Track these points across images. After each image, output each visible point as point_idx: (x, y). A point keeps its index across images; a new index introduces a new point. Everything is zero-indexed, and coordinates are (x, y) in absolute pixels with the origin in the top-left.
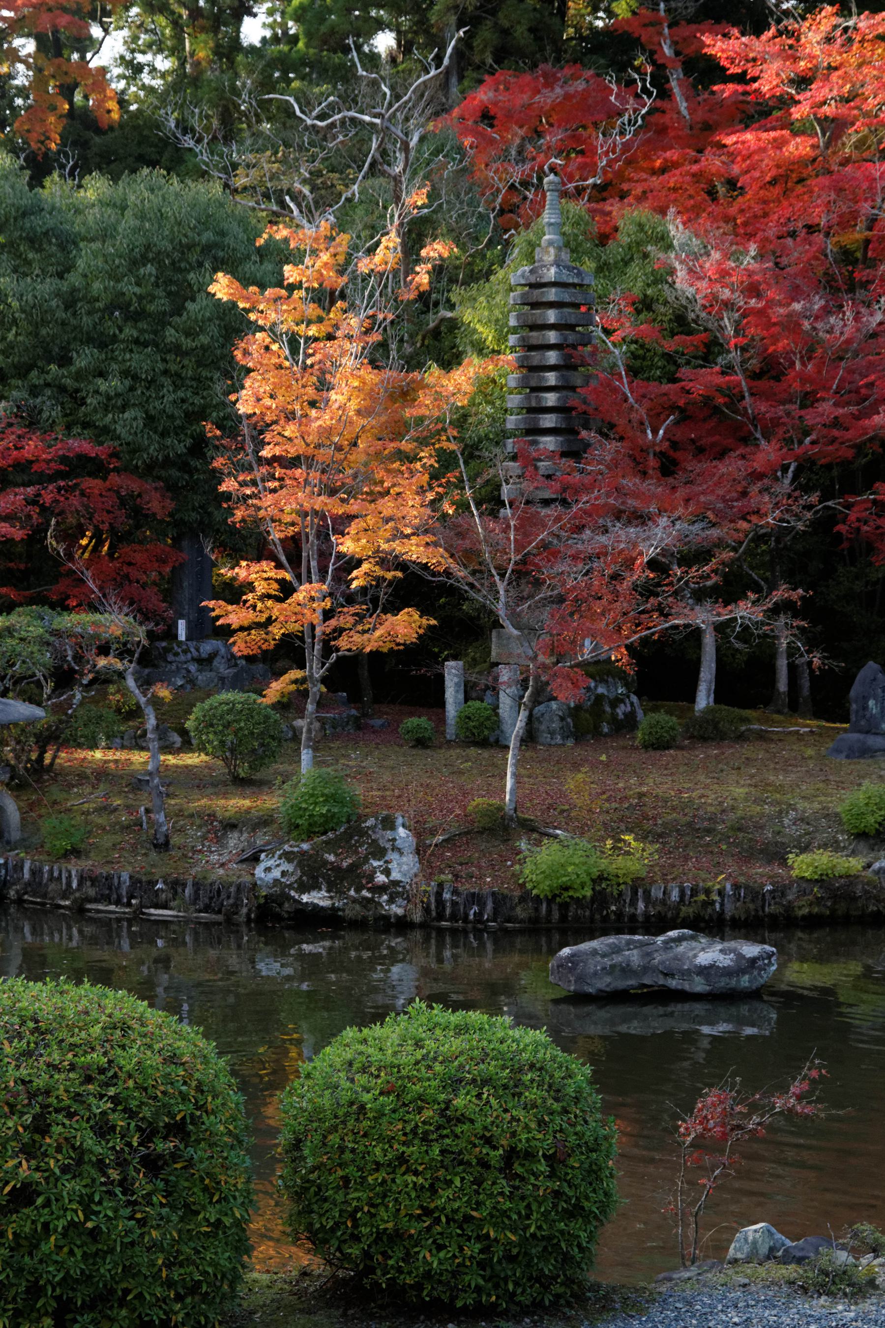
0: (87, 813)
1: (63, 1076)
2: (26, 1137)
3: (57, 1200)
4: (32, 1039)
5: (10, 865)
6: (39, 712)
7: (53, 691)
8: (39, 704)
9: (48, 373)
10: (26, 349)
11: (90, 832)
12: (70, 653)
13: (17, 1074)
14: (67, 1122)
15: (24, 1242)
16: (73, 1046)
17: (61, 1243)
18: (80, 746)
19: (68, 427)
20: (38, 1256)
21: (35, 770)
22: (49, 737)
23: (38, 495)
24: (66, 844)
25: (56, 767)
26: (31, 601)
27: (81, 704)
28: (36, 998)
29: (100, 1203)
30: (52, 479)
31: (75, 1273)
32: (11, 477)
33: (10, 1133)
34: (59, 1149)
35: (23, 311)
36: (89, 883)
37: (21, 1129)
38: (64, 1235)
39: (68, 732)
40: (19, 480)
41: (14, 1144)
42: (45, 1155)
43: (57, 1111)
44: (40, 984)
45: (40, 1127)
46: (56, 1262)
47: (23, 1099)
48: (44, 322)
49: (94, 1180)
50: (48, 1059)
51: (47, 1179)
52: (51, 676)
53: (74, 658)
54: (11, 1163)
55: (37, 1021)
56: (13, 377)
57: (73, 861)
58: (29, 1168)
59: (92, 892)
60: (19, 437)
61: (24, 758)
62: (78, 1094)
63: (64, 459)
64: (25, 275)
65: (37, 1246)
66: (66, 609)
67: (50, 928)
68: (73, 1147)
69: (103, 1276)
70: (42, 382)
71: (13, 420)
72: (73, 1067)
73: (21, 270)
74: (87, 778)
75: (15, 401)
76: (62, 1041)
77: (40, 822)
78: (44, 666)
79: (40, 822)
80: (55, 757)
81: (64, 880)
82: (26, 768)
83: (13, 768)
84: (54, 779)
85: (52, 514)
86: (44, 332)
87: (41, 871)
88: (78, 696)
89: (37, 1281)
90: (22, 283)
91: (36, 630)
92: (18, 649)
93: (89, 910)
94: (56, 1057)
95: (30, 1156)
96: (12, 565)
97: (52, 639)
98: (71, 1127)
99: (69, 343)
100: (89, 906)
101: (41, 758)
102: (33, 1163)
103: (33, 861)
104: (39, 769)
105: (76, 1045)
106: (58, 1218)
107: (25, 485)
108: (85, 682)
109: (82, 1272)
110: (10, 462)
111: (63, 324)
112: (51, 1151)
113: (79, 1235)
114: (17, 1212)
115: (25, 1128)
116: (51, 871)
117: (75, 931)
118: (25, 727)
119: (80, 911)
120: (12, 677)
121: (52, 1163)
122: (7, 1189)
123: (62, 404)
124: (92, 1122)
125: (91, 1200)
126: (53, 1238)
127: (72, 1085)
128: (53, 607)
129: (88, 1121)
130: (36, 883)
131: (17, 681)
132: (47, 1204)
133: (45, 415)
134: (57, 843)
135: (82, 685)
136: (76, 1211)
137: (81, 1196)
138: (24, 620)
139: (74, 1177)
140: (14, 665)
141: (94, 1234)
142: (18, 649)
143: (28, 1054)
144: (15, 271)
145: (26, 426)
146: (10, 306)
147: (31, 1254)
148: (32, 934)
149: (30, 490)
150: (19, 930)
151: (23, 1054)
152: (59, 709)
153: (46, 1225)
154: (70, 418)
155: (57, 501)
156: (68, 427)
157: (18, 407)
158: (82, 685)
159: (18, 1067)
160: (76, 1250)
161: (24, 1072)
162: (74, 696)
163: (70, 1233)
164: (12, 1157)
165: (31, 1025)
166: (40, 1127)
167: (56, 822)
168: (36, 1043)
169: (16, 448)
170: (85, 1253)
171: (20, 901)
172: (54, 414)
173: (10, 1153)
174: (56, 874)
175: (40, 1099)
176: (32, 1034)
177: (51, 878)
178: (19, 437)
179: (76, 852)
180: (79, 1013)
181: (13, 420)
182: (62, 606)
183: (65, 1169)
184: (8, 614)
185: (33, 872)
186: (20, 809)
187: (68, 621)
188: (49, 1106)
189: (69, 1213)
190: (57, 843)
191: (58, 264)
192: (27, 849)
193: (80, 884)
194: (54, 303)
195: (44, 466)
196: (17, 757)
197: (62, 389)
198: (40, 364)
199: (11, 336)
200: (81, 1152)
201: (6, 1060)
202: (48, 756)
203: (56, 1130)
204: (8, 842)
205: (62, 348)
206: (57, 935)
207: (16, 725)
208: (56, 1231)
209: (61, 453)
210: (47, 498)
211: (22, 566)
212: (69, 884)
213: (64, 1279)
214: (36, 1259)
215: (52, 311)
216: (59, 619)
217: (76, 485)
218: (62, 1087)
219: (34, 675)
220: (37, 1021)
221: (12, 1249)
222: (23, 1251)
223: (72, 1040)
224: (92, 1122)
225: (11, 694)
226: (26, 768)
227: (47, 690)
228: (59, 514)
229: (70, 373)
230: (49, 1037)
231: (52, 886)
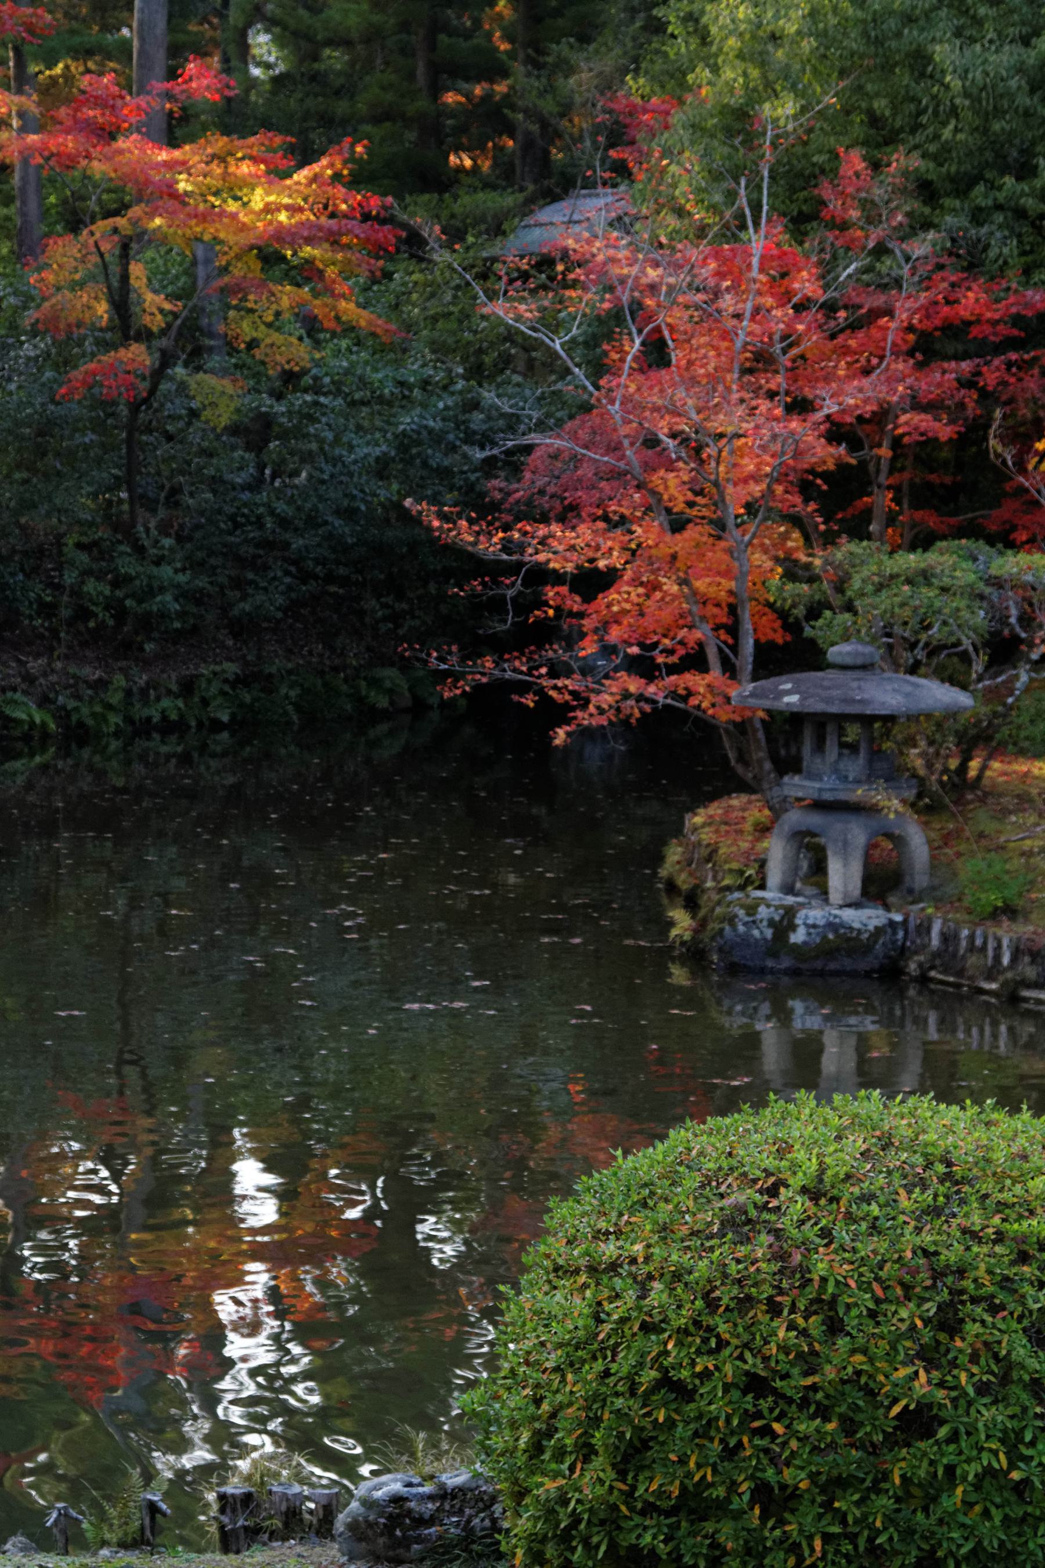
0: (1028, 854)
1: (985, 1249)
2: (927, 1336)
3: (968, 1434)
4: (942, 1189)
5: (912, 924)
6: (963, 699)
7: (987, 668)
8: (964, 687)
9: (1000, 188)
10: (970, 154)
11: (1032, 882)
12: (1014, 612)
13: (918, 1240)
14: (989, 1320)
15: (916, 1491)
16: (1002, 1206)
17: (973, 1497)
18: (1022, 753)
19: (1027, 272)
20: (937, 1513)
21: (954, 785)
22: (977, 737)
23: (978, 374)
24: (994, 898)
25: (985, 782)
26: (960, 532)
27: (1027, 690)
28: (950, 1129)
29: (1032, 1444)
30: (999, 349)
31: (991, 1545)
32: (937, 346)
33: (904, 1327)
34: (974, 1358)
35: (966, 94)
36: (1027, 959)
37: (919, 1323)
38: (977, 1487)
39: (1005, 731)
40: (950, 350)
41: (908, 1344)
42: (954, 1364)
43: (974, 1301)
44: (955, 1108)
45: (948, 1323)
46: (963, 1525)
47: (924, 1278)
48: (998, 113)
49: (1025, 1410)
50: (965, 1223)
51: (954, 1400)
52: (986, 644)
53: (1020, 619)
54: (903, 1372)
55: (949, 1164)
56: (948, 195)
57: (1006, 923)
58: (929, 1382)
59: (1031, 972)
60: (953, 285)
61: (938, 766)
62: (1007, 1279)
63: (1018, 320)
64: (973, 40)
65: (935, 1499)
66: (1011, 545)
67: (965, 1022)
68: (996, 1356)
69: (1032, 1553)
70: (990, 202)
71: (945, 260)
72: (1000, 1237)
73: (968, 33)
74: (1031, 801)
75: (949, 231)
76: (986, 1196)
77: (959, 863)
78: (975, 630)
79: (959, 863)
80: (984, 768)
81: (990, 953)
82: (940, 782)
83: (922, 781)
84: (983, 800)
85: (997, 401)
86: (997, 126)
87: (956, 936)
88: (1024, 678)
89: (933, 1551)
90: (968, 53)
91: (966, 575)
92: (937, 604)
93: (1026, 1000)
94: (976, 1220)
95: (931, 1364)
96: (933, 478)
97: (988, 590)
98: (994, 1326)
99: (1033, 143)
100: (1026, 993)
101: (963, 768)
102: (936, 1374)
103: (945, 921)
104: (960, 785)
105: (1006, 1205)
106: (968, 1461)
107: (958, 358)
108: (1034, 656)
109: (1002, 1543)
110: (937, 322)
111: (1027, 113)
112: (963, 1359)
113: (1001, 1489)
114: (908, 1445)
115: (927, 1322)
116: (972, 937)
117: (1003, 1028)
118: (941, 722)
119: (1011, 999)
120: (927, 644)
121: (963, 1377)
122: (896, 1410)
123: (1019, 236)
124: (1026, 1322)
125: (1020, 1439)
126: (959, 1490)
127: (999, 1264)
128: (991, 542)
129: (1020, 1319)
130: (948, 955)
131: (933, 651)
132: (954, 1437)
133: (992, 253)
134: (983, 896)
135: (1029, 661)
136: (995, 1453)
137: (1005, 1431)
138: (949, 560)
139: (995, 1402)
140: (929, 627)
141: (1021, 1488)
142: (937, 604)
143: (935, 1211)
144: (958, 33)
145: (964, 269)
146: (947, 87)
147: (926, 1510)
148: (939, 1031)
149: (966, 366)
150: (921, 1023)
151: (926, 1212)
152: (993, 695)
153: (950, 1469)
154: (1029, 258)
155: (1005, 383)
156: (1027, 272)
157: (953, 240)
158: (1029, 661)
159: (918, 1230)
160: (993, 1510)
161: (927, 1238)
162: (1017, 677)
163: (986, 1484)
164: (904, 1364)
165: (941, 1168)
166: (948, 1323)
167: (982, 865)
168: (947, 1197)
169: (948, 302)
170: (1006, 1518)
171: (923, 980)
172: (1006, 251)
173: (901, 1357)
174: (978, 942)
175: (949, 1280)
176: (942, 1182)
177: (971, 948)
178: (953, 285)
179: (1010, 911)
180: (1013, 1157)
181: (945, 260)
182: (1005, 540)
183: (982, 1389)
184: (925, 550)
185: (945, 938)
186: (929, 842)
187: (1012, 564)
188: (962, 1292)
189: (985, 1455)
190: (983, 896)
191: (1023, 23)
192: (938, 902)
193: (1014, 959)
194: (1013, 83)
195: (987, 329)
196: (929, 766)
197: (1021, 213)
198: (988, 175)
199: (947, 133)
200: (1007, 1367)
201: (902, 1218)
202: (974, 765)
203: (973, 1329)
204: (910, 891)
205: (1022, 151)
206: (975, 1031)
207: (929, 716)
208: (964, 1479)
209: (1014, 310)
210: (990, 378)
211: (948, 480)
212: (997, 958)
213: (973, 1552)
214: (933, 1519)
215: (1011, 96)
216: (1000, 561)
217: (1035, 359)
218: (983, 1267)
219: (958, 643)
220: (949, 1164)
221: (898, 1500)
222: (914, 1503)
223: (1000, 1197)
224: (1026, 1322)
225: (923, 670)
226: (940, 782)
227: (978, 667)
228: (1006, 403)
229: (1033, 189)
230: (966, 1188)
231: (973, 960)
